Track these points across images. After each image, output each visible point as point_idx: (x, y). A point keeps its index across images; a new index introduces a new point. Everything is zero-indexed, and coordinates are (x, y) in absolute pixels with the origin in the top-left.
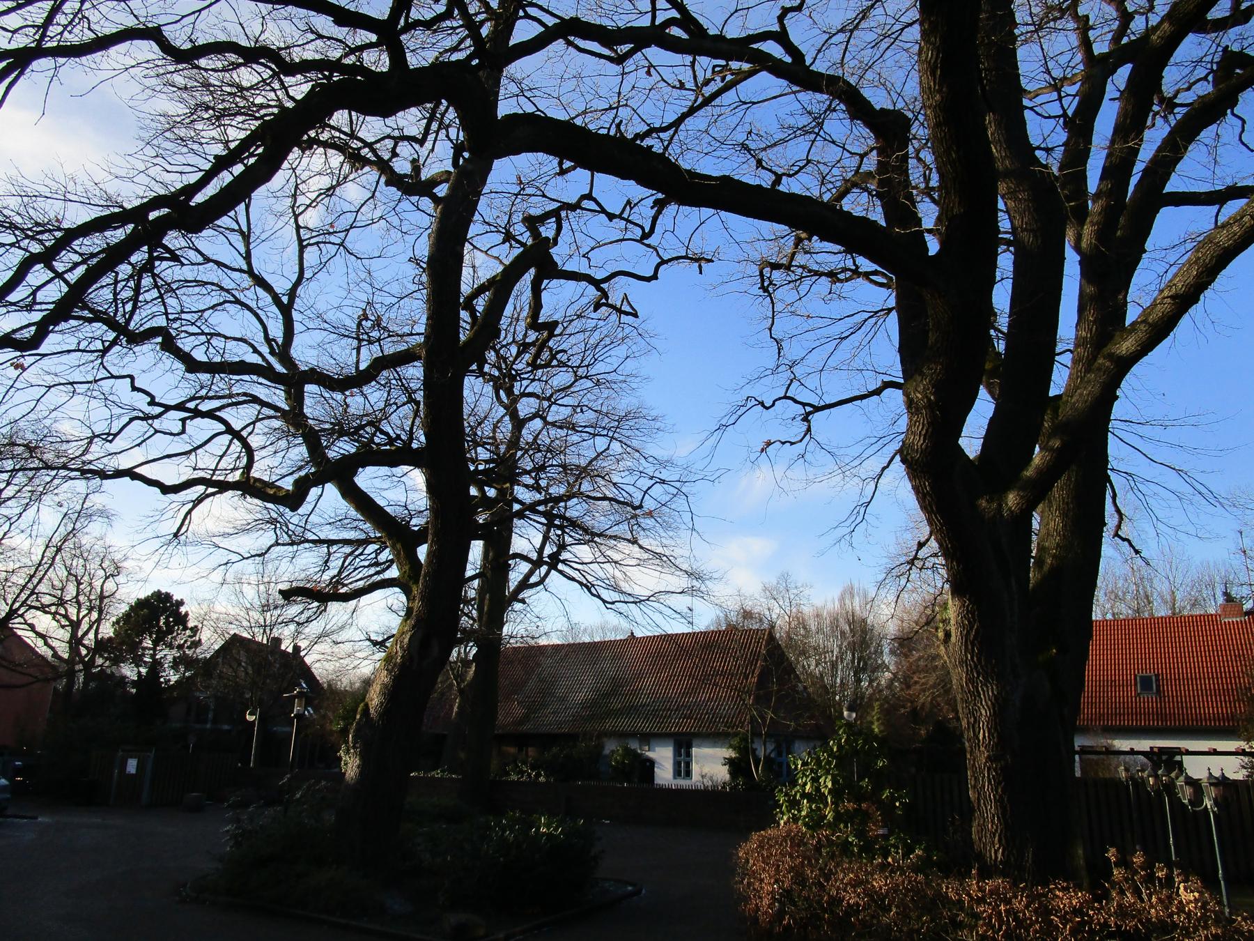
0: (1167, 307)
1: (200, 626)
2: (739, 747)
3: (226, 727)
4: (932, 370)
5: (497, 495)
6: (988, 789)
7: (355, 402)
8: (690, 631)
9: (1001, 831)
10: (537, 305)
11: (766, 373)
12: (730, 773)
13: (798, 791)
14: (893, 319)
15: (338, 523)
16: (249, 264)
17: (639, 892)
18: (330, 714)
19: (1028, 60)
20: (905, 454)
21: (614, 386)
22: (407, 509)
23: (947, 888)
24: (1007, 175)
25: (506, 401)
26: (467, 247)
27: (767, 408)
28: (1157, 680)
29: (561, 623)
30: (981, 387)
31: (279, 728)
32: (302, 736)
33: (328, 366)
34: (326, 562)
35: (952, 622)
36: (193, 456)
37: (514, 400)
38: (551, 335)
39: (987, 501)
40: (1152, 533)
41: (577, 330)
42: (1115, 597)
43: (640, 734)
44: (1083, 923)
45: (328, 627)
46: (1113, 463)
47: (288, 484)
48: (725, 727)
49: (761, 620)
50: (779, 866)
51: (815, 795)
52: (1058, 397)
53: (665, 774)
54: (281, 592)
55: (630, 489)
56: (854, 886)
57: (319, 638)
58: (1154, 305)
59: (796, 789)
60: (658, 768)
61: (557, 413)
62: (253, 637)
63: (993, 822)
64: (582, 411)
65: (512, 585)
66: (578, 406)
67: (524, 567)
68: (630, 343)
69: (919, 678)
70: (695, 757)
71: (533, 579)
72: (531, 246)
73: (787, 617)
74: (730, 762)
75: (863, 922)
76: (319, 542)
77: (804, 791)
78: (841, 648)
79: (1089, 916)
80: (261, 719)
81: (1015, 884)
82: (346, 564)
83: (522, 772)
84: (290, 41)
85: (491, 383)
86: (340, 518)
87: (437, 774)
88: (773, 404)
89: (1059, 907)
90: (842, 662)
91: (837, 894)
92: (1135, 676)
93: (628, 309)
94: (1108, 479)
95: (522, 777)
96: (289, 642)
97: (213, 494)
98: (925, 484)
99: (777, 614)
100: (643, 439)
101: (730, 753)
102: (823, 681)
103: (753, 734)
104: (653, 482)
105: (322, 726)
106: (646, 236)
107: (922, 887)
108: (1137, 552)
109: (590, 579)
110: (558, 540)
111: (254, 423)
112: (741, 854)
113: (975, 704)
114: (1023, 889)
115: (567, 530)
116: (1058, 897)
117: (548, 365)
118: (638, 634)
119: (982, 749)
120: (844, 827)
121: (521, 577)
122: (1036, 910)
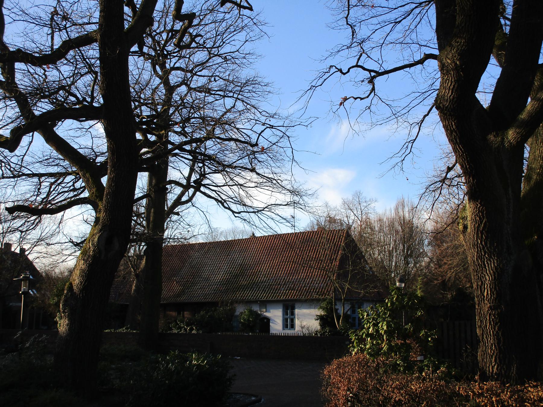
2: (327, 308)
4: (458, 43)
5: (157, 139)
6: (489, 328)
7: (53, 74)
8: (293, 231)
9: (497, 354)
11: (343, 48)
13: (364, 332)
15: (46, 161)
17: (260, 400)
18: (48, 293)
20: (438, 104)
21: (237, 62)
22: (94, 151)
23: (459, 388)
25: (160, 73)
27: (344, 74)
29: (204, 229)
30: (492, 57)
31: (14, 304)
32: (30, 308)
33: (30, 46)
34: (39, 189)
35: (469, 219)
37: (167, 73)
38: (190, 25)
39: (494, 136)
41: (210, 22)
43: (259, 301)
45: (43, 235)
48: (317, 294)
49: (342, 224)
51: (376, 335)
54: (7, 209)
55: (249, 133)
56: (399, 389)
57: (37, 242)
59: (363, 332)
60: (272, 323)
61: (198, 82)
63: (491, 349)
64: (215, 80)
65: (170, 203)
66: (212, 76)
67: (178, 190)
68: (248, 30)
69: (447, 261)
70: (297, 315)
71: (184, 199)
73: (359, 222)
74: (321, 318)
76: (33, 175)
77: (368, 332)
78: (395, 241)
81: (504, 384)
82: (52, 189)
83: (180, 328)
85: (150, 61)
86: (46, 158)
87: (123, 330)
88: (348, 71)
89: (530, 397)
90: (396, 251)
91: (388, 394)
93: (246, 4)
95: (181, 331)
96: (16, 245)
98: (452, 124)
100: (259, 99)
102: (383, 263)
103: (336, 299)
104: (265, 127)
105: (43, 301)
107: (443, 388)
109: (224, 197)
110: (200, 170)
112: (325, 373)
113: (482, 273)
114: (508, 387)
115: (207, 164)
116: (529, 391)
117: (188, 46)
118: (258, 234)
119: (486, 302)
120: (394, 355)
121: (176, 197)
122: (515, 400)
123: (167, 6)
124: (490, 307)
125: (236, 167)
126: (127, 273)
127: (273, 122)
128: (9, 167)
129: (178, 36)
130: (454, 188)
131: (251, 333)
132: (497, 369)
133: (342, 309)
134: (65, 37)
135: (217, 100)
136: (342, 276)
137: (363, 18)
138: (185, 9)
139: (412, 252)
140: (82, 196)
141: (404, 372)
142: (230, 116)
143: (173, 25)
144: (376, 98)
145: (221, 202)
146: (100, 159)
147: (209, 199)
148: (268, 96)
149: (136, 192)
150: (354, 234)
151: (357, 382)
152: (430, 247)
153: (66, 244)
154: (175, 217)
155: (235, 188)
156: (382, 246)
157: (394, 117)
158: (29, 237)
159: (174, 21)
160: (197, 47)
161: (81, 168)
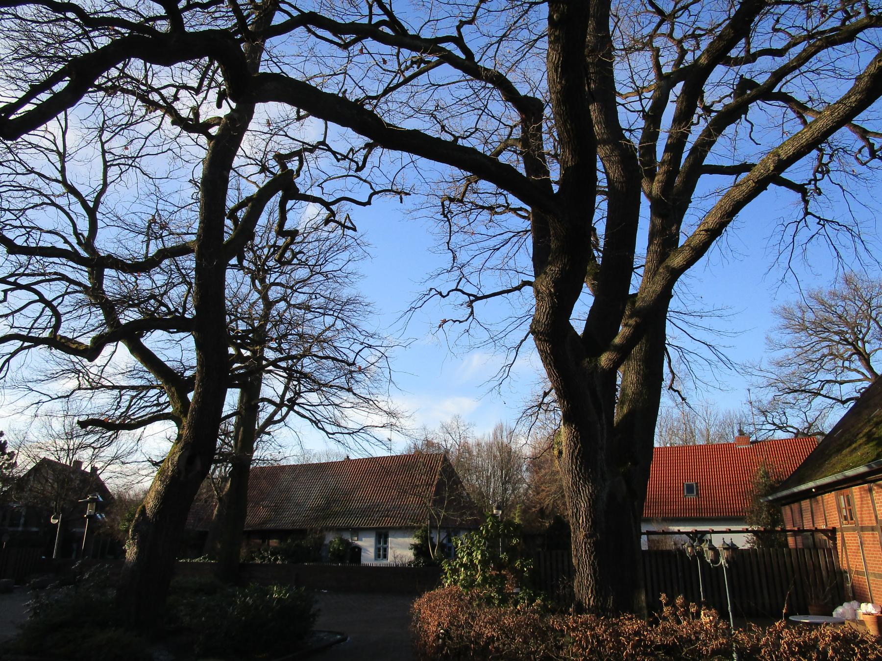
0: (703, 237)
1: (16, 452)
2: (421, 537)
3: (35, 529)
4: (553, 269)
7: (144, 283)
10: (283, 218)
12: (415, 555)
14: (529, 241)
15: (131, 373)
16: (64, 176)
18: (118, 518)
19: (620, 74)
20: (533, 331)
23: (553, 622)
24: (604, 142)
26: (232, 173)
27: (444, 297)
28: (697, 487)
29: (297, 450)
30: (585, 285)
33: (122, 253)
34: (119, 403)
35: (564, 444)
36: (10, 318)
37: (266, 288)
40: (693, 387)
41: (314, 240)
42: (673, 432)
44: (640, 641)
45: (119, 452)
46: (669, 340)
47: (86, 341)
49: (439, 448)
50: (441, 613)
52: (635, 295)
53: (369, 556)
54: (79, 422)
58: (694, 235)
62: (59, 460)
67: (271, 409)
68: (352, 251)
71: (277, 418)
72: (280, 175)
73: (457, 446)
74: (415, 547)
75: (497, 649)
76: (114, 387)
77: (462, 562)
79: (644, 635)
80: (63, 522)
82: (132, 403)
83: (263, 558)
84: (98, 9)
86: (130, 369)
88: (448, 294)
90: (494, 477)
92: (683, 484)
93: (350, 225)
94: (666, 349)
97: (29, 347)
99: (449, 443)
100: (359, 318)
101: (415, 541)
105: (112, 527)
106: (359, 169)
108: (683, 399)
109: (319, 417)
111: (63, 296)
115: (302, 382)
116: (625, 624)
117: (289, 263)
118: (352, 457)
119: (581, 530)
121: (268, 415)
122: (610, 634)
123: (271, 222)
124: (586, 535)
125: (331, 386)
126: (209, 497)
127: (371, 342)
128: (87, 378)
129: (280, 251)
130: (552, 413)
131: (341, 563)
132: (593, 601)
133: (437, 537)
134: (161, 246)
135: (316, 317)
136: (438, 502)
137: (464, 244)
138: (288, 226)
139: (510, 478)
140: (166, 411)
141: (499, 605)
142: (329, 334)
143: (276, 240)
144: (474, 322)
145: (315, 422)
146: (188, 373)
147: (303, 419)
148: (369, 316)
149: (224, 410)
150: (452, 459)
151: (448, 617)
152: (528, 474)
153: (144, 463)
154: (265, 437)
155: (330, 408)
156: (480, 472)
157: (491, 340)
158: (102, 454)
159: (277, 237)
160: (299, 264)
161: (166, 382)
